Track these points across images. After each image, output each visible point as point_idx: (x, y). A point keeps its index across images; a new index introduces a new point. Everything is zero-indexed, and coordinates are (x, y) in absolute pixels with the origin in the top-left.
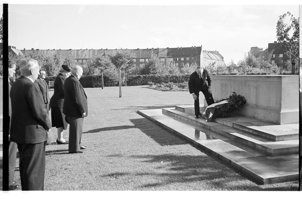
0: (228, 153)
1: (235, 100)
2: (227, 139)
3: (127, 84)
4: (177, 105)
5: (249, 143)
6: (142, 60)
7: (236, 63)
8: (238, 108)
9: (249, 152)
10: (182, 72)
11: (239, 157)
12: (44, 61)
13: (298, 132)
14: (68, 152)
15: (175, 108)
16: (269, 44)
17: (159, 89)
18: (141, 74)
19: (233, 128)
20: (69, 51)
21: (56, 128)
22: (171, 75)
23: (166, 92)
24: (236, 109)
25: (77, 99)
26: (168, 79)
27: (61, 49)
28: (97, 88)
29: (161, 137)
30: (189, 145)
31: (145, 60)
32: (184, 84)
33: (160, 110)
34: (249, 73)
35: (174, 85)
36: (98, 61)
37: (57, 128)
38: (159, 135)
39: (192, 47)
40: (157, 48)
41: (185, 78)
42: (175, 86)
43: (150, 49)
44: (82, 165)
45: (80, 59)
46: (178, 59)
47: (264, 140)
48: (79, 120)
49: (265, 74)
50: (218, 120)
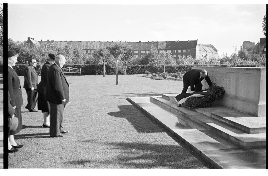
0: (200, 143)
1: (215, 91)
2: (203, 129)
3: (127, 73)
4: (165, 93)
5: (224, 134)
6: (143, 52)
7: (229, 56)
8: (218, 99)
9: (222, 143)
10: (178, 63)
11: (210, 148)
12: (56, 51)
13: (265, 126)
14: (49, 135)
15: (161, 96)
16: (260, 38)
17: (154, 78)
18: (140, 64)
19: (211, 118)
20: (79, 42)
21: (42, 112)
22: (166, 65)
23: (160, 80)
24: (216, 99)
25: (56, 87)
26: (164, 69)
28: (99, 76)
29: (141, 124)
30: (166, 134)
31: (146, 52)
32: (177, 74)
33: (148, 98)
34: (240, 65)
35: (168, 75)
36: (101, 52)
37: (43, 113)
38: (140, 122)
39: (189, 40)
40: (253, 42)
41: (181, 69)
42: (168, 76)
44: (57, 149)
45: (89, 50)
47: (237, 131)
48: (60, 107)
49: (255, 66)
50: (198, 109)
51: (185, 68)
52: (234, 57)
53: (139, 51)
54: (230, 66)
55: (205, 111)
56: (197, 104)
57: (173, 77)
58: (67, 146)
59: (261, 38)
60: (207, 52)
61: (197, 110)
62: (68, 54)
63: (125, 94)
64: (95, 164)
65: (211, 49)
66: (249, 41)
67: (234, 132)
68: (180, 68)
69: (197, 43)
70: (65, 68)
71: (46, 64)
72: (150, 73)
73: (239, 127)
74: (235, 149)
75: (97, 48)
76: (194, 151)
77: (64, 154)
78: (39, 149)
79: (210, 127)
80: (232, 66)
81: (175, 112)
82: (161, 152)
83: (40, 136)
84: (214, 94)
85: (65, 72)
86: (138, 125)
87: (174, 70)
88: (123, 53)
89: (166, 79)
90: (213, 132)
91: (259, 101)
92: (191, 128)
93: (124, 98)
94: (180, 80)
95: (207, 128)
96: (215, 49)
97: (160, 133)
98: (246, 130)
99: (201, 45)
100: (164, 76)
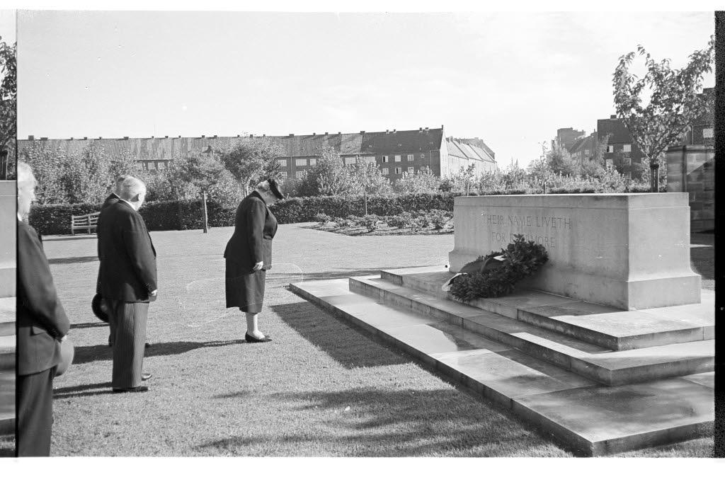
0: (506, 381)
2: (503, 349)
4: (385, 268)
5: (557, 357)
6: (301, 162)
7: (525, 166)
8: (530, 274)
10: (397, 189)
11: (531, 392)
14: (111, 389)
15: (379, 276)
22: (371, 196)
23: (358, 237)
25: (139, 259)
26: (364, 207)
27: (103, 138)
31: (308, 162)
32: (401, 219)
33: (345, 282)
34: (555, 189)
39: (421, 129)
40: (580, 130)
42: (380, 224)
44: (148, 423)
45: (150, 161)
47: (587, 346)
49: (592, 191)
51: (418, 202)
52: (537, 173)
53: (291, 159)
54: (533, 194)
57: (393, 226)
58: (173, 412)
60: (468, 158)
61: (480, 306)
62: (93, 173)
63: (280, 277)
64: (261, 448)
65: (478, 150)
66: (572, 128)
67: (580, 350)
68: (406, 202)
69: (442, 135)
70: (94, 214)
71: (110, 202)
75: (179, 157)
76: (493, 400)
77: (172, 432)
78: (100, 425)
79: (521, 343)
80: (538, 193)
81: (424, 314)
83: (77, 393)
84: (519, 263)
86: (340, 350)
89: (376, 232)
92: (474, 348)
93: (280, 285)
94: (412, 234)
95: (512, 346)
96: (488, 150)
97: (401, 365)
98: (606, 343)
99: (452, 141)
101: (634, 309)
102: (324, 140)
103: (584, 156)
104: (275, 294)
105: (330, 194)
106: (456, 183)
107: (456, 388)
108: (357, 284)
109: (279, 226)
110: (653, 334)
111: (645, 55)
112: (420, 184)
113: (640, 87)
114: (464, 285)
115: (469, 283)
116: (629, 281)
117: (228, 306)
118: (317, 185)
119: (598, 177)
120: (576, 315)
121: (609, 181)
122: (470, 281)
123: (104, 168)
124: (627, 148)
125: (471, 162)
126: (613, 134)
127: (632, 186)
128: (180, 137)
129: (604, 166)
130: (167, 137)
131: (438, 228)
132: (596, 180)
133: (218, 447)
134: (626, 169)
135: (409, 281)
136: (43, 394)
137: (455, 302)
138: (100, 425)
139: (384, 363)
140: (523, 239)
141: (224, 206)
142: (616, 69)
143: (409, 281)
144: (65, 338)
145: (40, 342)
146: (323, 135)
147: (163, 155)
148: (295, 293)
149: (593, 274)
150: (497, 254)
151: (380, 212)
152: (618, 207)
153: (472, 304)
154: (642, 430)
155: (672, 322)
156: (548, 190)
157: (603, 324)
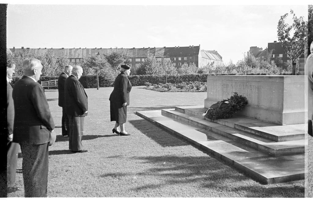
2: (229, 140)
5: (252, 144)
6: (138, 60)
7: (235, 63)
10: (179, 72)
11: (241, 158)
15: (174, 109)
17: (156, 90)
19: (235, 129)
22: (169, 75)
23: (164, 93)
25: (78, 99)
26: (166, 80)
27: (53, 48)
29: (162, 138)
30: (191, 146)
31: (141, 60)
32: (182, 85)
33: (160, 111)
34: (249, 73)
40: (260, 48)
42: (173, 87)
43: (147, 49)
45: (73, 58)
46: (175, 58)
47: (263, 139)
50: (220, 121)
52: (241, 66)
55: (227, 122)
56: (217, 115)
59: (270, 43)
61: (218, 122)
66: (256, 47)
67: (262, 141)
70: (50, 81)
71: (62, 75)
72: (151, 84)
73: (265, 136)
74: (264, 157)
79: (236, 138)
81: (194, 125)
82: (193, 164)
85: (50, 85)
87: (178, 81)
88: (123, 62)
89: (171, 90)
90: (240, 142)
91: (283, 110)
95: (232, 139)
98: (274, 138)
99: (203, 51)
100: (168, 87)
101: (285, 125)
102: (148, 51)
103: (261, 59)
104: (131, 116)
105: (151, 74)
106: (205, 70)
107: (209, 156)
108: (166, 113)
109: (132, 87)
110: (293, 135)
111: (293, 14)
112: (191, 71)
113: (289, 29)
114: (212, 113)
115: (214, 113)
116: (283, 113)
117: (111, 121)
118: (145, 70)
119: (268, 68)
120: (260, 127)
121: (273, 70)
122: (214, 111)
123: (54, 61)
124: (281, 56)
125: (212, 61)
126: (274, 49)
127: (283, 73)
128: (86, 48)
129: (271, 63)
130: (80, 48)
131: (198, 89)
132: (267, 70)
133: (112, 177)
134: (281, 65)
135: (188, 111)
136: (45, 154)
137: (208, 120)
138: (63, 167)
139: (178, 145)
140: (237, 95)
141: (106, 78)
142: (279, 21)
143: (188, 111)
144: (53, 131)
145: (44, 132)
146: (147, 48)
147: (78, 56)
148: (138, 115)
149: (267, 110)
150: (226, 101)
151: (173, 82)
152: (280, 81)
153: (215, 121)
154: (289, 174)
155: (301, 131)
156: (246, 73)
157: (271, 131)
